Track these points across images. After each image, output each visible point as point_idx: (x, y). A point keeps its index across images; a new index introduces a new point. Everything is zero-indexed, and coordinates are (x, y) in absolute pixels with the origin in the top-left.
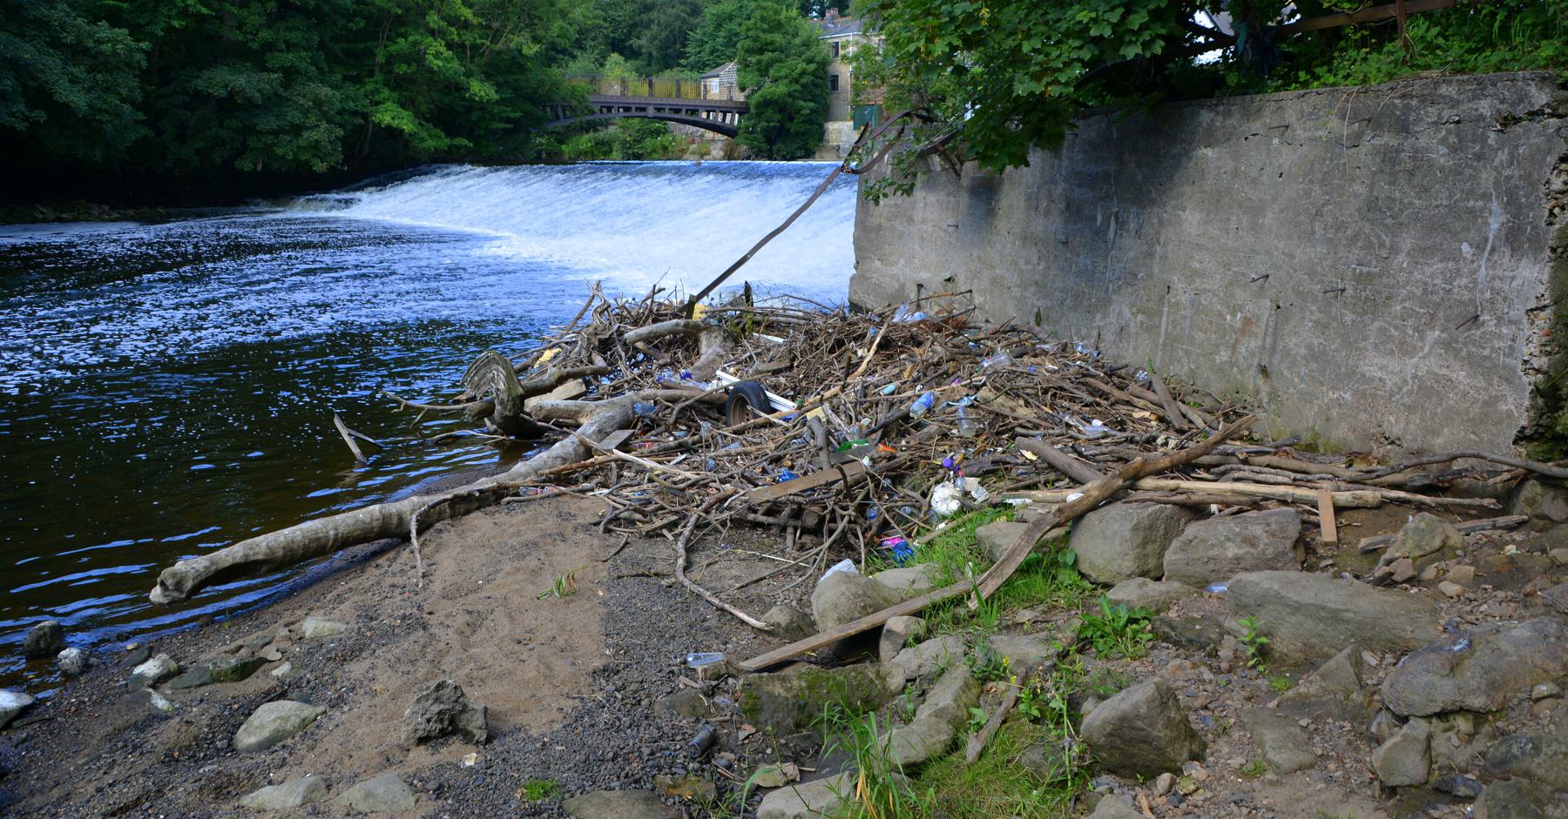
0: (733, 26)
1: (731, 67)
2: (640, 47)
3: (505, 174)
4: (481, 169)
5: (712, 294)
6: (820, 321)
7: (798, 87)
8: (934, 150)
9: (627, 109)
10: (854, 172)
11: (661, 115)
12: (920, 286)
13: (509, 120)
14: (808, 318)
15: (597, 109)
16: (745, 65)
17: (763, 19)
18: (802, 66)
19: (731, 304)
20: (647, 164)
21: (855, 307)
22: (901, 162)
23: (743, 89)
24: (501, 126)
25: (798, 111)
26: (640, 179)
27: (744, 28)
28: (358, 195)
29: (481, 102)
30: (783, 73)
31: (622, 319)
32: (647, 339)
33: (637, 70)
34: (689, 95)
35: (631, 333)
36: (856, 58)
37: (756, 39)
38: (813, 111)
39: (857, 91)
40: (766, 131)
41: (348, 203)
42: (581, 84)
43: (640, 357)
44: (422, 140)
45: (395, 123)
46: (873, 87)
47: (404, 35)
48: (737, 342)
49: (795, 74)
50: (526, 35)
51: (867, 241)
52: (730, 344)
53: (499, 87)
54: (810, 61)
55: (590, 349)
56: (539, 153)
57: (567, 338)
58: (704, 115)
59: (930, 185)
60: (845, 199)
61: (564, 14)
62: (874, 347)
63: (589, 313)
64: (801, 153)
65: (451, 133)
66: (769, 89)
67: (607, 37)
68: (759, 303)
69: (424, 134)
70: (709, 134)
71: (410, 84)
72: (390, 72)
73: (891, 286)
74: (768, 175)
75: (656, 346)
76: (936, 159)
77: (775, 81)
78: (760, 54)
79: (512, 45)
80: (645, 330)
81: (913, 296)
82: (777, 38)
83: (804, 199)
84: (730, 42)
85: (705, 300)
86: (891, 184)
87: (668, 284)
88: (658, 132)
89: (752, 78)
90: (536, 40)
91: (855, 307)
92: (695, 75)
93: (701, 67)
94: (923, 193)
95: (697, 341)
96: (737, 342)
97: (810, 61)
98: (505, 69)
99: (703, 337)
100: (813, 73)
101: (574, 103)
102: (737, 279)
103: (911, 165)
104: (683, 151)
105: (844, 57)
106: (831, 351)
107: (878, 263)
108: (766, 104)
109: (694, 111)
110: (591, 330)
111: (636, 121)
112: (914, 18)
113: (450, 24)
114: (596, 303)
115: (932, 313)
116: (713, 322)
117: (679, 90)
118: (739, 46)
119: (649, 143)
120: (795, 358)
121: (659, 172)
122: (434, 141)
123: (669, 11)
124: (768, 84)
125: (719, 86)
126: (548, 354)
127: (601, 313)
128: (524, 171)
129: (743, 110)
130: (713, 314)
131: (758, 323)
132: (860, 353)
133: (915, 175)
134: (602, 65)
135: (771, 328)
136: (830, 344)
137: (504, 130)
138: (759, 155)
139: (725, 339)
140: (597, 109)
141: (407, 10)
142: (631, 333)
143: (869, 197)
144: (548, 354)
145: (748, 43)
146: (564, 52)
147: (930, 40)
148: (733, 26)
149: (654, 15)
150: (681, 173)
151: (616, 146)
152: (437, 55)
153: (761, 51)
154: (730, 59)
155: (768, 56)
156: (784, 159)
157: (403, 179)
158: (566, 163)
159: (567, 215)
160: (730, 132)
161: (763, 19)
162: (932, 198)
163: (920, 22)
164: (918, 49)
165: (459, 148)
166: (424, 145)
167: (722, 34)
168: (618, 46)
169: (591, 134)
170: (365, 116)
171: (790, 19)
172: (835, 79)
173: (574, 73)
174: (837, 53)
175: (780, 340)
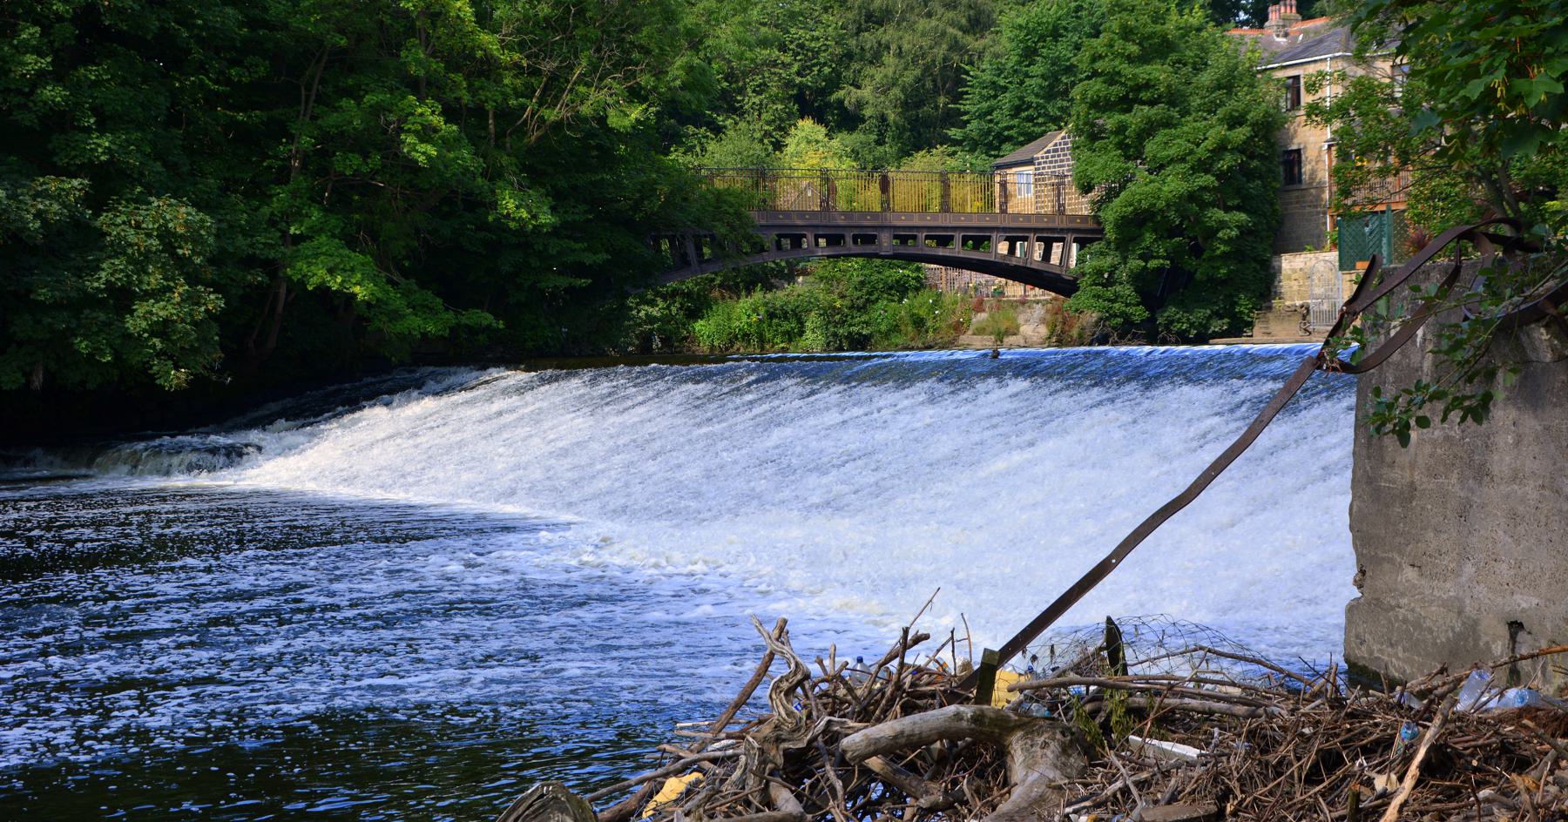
0: (1062, 49)
1: (1059, 139)
2: (860, 104)
3: (575, 385)
4: (518, 377)
5: (1034, 647)
6: (1282, 709)
7: (1207, 180)
8: (1534, 315)
9: (834, 240)
10: (1346, 367)
11: (910, 249)
12: (1515, 627)
13: (580, 270)
14: (1253, 700)
15: (769, 239)
16: (1092, 135)
17: (1127, 33)
18: (1217, 132)
19: (1076, 668)
20: (879, 357)
21: (1361, 675)
22: (1457, 345)
23: (1086, 189)
24: (564, 282)
25: (1211, 233)
26: (866, 391)
27: (1085, 55)
28: (254, 436)
29: (521, 232)
30: (1172, 152)
31: (834, 705)
32: (892, 750)
33: (855, 155)
34: (968, 201)
35: (856, 738)
36: (1340, 109)
37: (1112, 78)
38: (1245, 231)
39: (1346, 182)
40: (1138, 279)
41: (234, 455)
42: (732, 182)
43: (877, 790)
44: (395, 316)
45: (335, 283)
46: (1384, 172)
47: (355, 93)
48: (1092, 755)
49: (1201, 152)
50: (615, 84)
51: (1380, 524)
52: (1077, 761)
53: (559, 200)
54: (1234, 122)
55: (766, 775)
56: (647, 339)
57: (714, 749)
58: (1003, 248)
59: (1531, 394)
60: (1329, 429)
61: (695, 41)
62: (1413, 770)
63: (763, 693)
64: (1217, 325)
65: (455, 300)
66: (1144, 187)
67: (789, 84)
68: (1141, 664)
69: (397, 301)
70: (1015, 290)
71: (365, 198)
72: (323, 172)
73: (1443, 625)
74: (1146, 377)
75: (911, 767)
76: (1542, 335)
77: (1158, 168)
78: (1122, 116)
79: (585, 110)
80: (886, 729)
81: (1499, 649)
82: (1159, 73)
83: (1232, 431)
84: (1055, 89)
85: (1018, 661)
86: (1436, 396)
87: (936, 624)
88: (901, 289)
89: (1107, 162)
90: (636, 95)
91: (1361, 675)
92: (980, 160)
93: (992, 143)
94: (1513, 413)
95: (1002, 755)
96: (1092, 755)
97: (1234, 122)
98: (572, 161)
99: (1017, 747)
100: (1241, 149)
101: (721, 230)
102: (1088, 614)
103: (1487, 349)
104: (958, 328)
105: (1314, 110)
106: (1312, 778)
107: (1410, 574)
108: (1136, 224)
109: (979, 239)
110: (766, 730)
111: (855, 263)
112: (1478, 24)
113: (453, 65)
114: (778, 670)
115: (1549, 690)
116: (1038, 710)
117: (945, 195)
118: (1076, 93)
119: (884, 311)
120: (1226, 794)
121: (905, 376)
122: (426, 321)
123: (922, 24)
124: (1141, 172)
125: (1027, 189)
126: (673, 787)
127: (790, 692)
128: (620, 379)
129: (1087, 236)
130: (1035, 692)
131: (1139, 713)
132: (1380, 783)
133: (1491, 375)
134: (778, 146)
135: (1170, 723)
136: (1308, 762)
137: (570, 290)
138: (1128, 331)
139: (1065, 750)
140: (769, 239)
141: (360, 37)
142: (856, 738)
143: (1382, 428)
144: (673, 787)
145: (1097, 87)
146: (698, 119)
147: (1518, 70)
148: (1062, 49)
149: (887, 34)
150: (958, 375)
151: (812, 320)
152: (427, 133)
153: (1125, 103)
154: (1057, 122)
155: (1138, 116)
156: (1183, 339)
157: (354, 404)
158: (704, 360)
159: (708, 475)
160: (1061, 285)
161: (1127, 33)
162: (1531, 424)
163: (1494, 33)
164: (1490, 91)
165: (472, 331)
166: (399, 327)
167: (1038, 69)
168: (815, 103)
169: (758, 296)
170: (272, 267)
171: (1186, 31)
172: (1293, 159)
173: (719, 156)
174: (1296, 102)
175: (1192, 752)
